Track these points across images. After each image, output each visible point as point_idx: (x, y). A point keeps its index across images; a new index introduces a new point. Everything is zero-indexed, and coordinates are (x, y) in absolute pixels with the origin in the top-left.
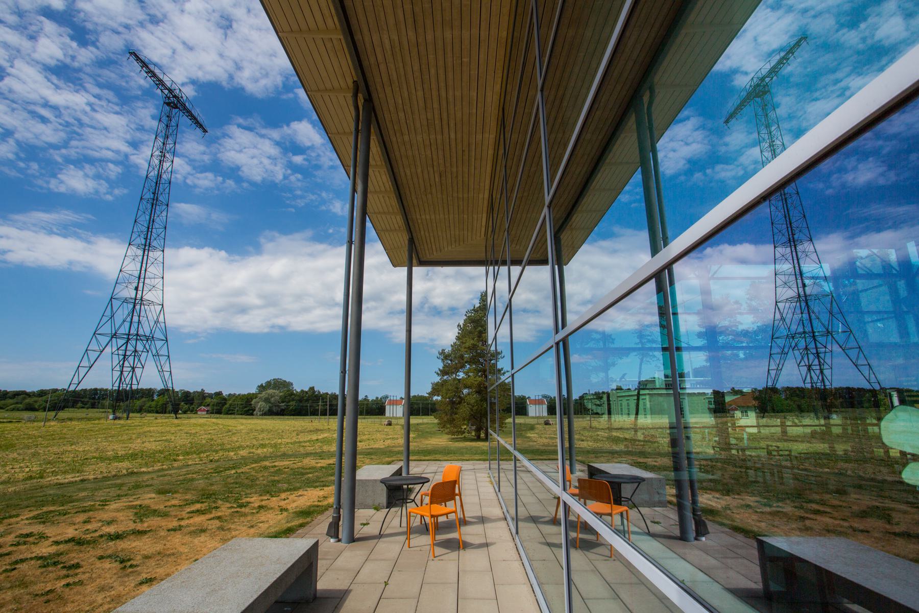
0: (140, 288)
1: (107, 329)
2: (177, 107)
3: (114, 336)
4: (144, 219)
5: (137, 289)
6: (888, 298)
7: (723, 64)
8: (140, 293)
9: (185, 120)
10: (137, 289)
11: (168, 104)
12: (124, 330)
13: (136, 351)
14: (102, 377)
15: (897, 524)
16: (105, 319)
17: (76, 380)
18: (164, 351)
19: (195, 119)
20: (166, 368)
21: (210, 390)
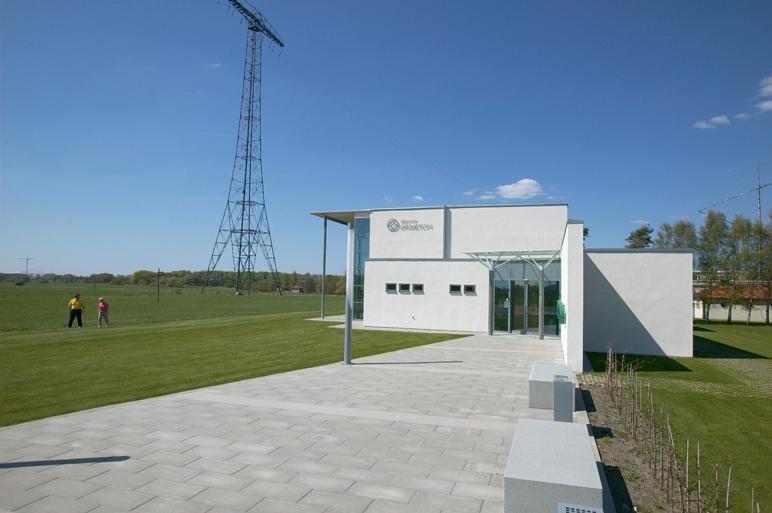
0: (247, 191)
1: (227, 226)
2: (258, 30)
3: (233, 231)
4: (240, 175)
5: (247, 150)
6: (527, 397)
7: (500, 187)
8: (247, 196)
9: (267, 40)
10: (247, 150)
11: (252, 29)
12: (239, 228)
13: (249, 243)
14: (227, 265)
15: (522, 303)
16: (225, 219)
17: (212, 266)
18: (268, 242)
19: (274, 37)
20: (271, 255)
21: (302, 272)
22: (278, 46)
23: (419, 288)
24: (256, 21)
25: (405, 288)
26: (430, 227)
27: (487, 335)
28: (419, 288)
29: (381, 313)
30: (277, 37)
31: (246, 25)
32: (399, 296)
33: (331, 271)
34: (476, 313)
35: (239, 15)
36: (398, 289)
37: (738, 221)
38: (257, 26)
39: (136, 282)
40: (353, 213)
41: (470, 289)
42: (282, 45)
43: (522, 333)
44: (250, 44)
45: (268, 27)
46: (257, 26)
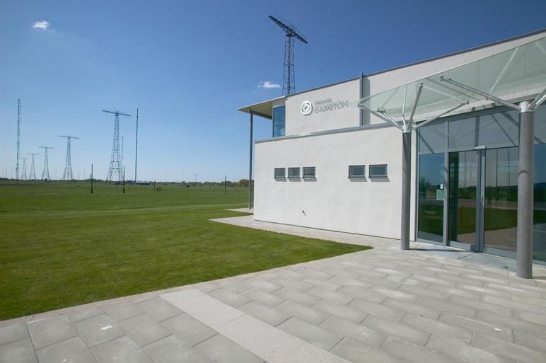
2: (291, 36)
9: (297, 41)
11: (288, 36)
22: (304, 43)
23: (310, 173)
24: (290, 30)
25: (294, 173)
26: (343, 104)
27: (398, 247)
28: (310, 173)
29: (274, 209)
30: (300, 35)
31: (285, 33)
32: (288, 184)
33: (511, 185)
34: (379, 212)
35: (280, 29)
36: (301, 175)
37: (427, 183)
38: (291, 33)
39: (240, 185)
40: (271, 103)
41: (379, 172)
42: (306, 43)
43: (474, 250)
44: (287, 44)
45: (297, 32)
46: (291, 33)
